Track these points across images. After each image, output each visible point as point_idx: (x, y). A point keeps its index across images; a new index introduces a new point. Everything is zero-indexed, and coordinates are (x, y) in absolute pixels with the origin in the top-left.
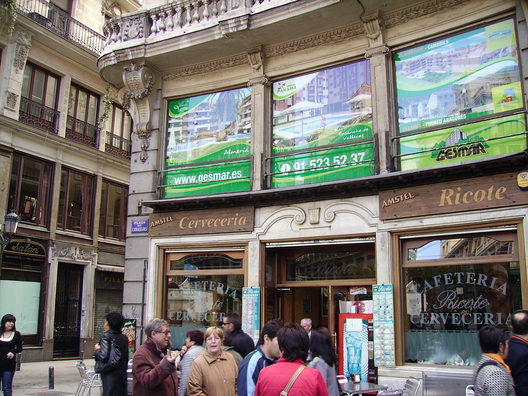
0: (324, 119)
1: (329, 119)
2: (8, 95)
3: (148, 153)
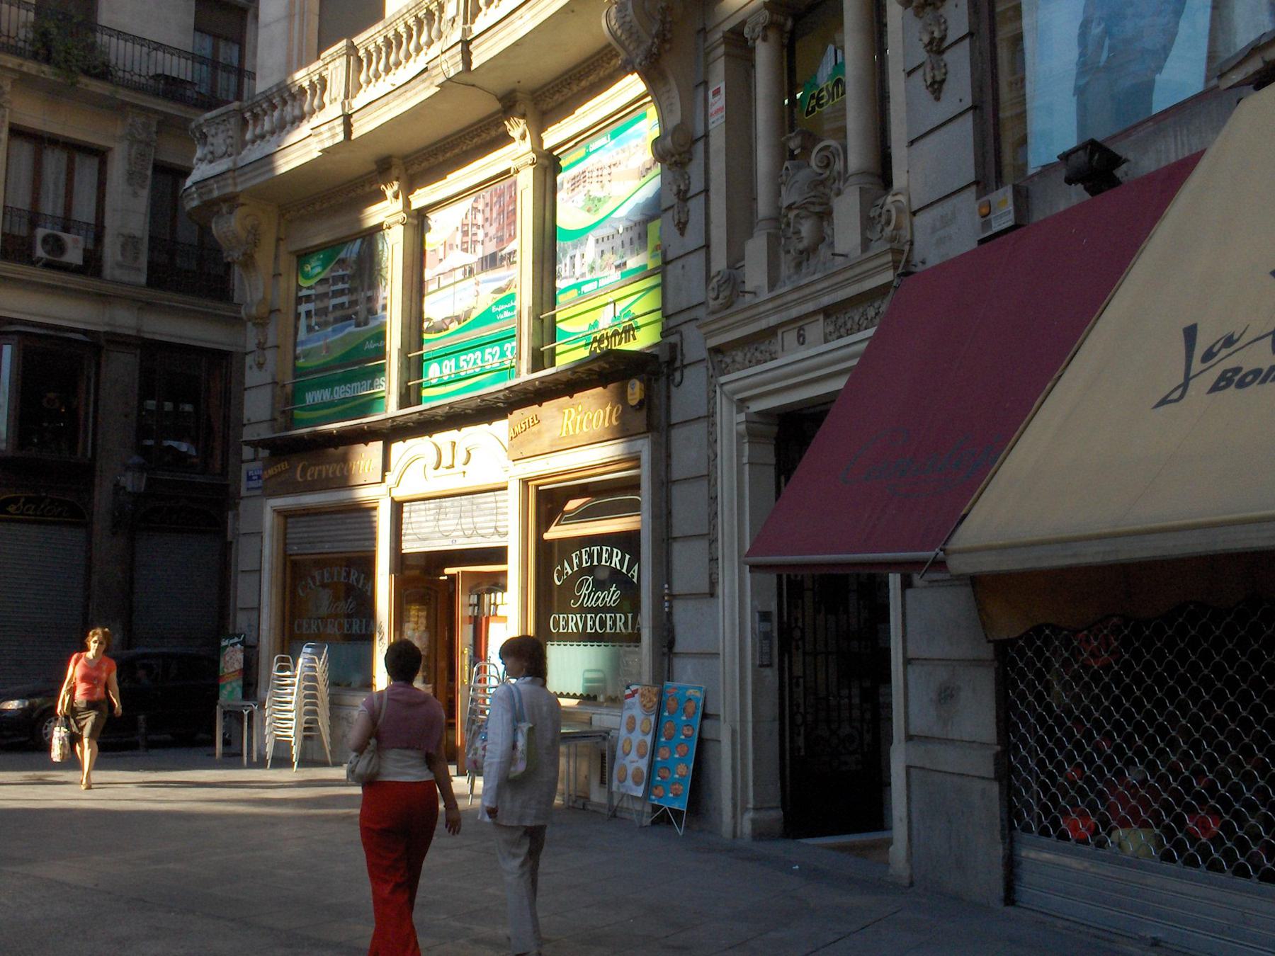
0: (477, 284)
1: (484, 282)
2: (121, 239)
3: (947, 56)
